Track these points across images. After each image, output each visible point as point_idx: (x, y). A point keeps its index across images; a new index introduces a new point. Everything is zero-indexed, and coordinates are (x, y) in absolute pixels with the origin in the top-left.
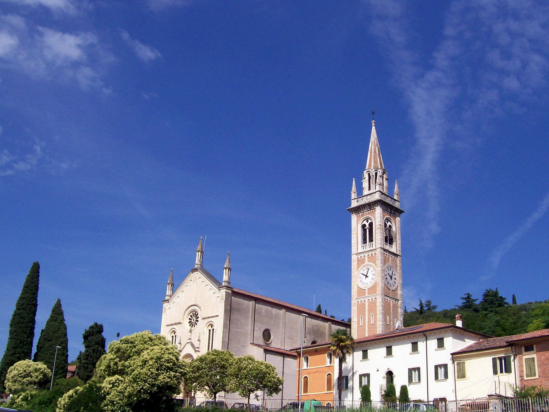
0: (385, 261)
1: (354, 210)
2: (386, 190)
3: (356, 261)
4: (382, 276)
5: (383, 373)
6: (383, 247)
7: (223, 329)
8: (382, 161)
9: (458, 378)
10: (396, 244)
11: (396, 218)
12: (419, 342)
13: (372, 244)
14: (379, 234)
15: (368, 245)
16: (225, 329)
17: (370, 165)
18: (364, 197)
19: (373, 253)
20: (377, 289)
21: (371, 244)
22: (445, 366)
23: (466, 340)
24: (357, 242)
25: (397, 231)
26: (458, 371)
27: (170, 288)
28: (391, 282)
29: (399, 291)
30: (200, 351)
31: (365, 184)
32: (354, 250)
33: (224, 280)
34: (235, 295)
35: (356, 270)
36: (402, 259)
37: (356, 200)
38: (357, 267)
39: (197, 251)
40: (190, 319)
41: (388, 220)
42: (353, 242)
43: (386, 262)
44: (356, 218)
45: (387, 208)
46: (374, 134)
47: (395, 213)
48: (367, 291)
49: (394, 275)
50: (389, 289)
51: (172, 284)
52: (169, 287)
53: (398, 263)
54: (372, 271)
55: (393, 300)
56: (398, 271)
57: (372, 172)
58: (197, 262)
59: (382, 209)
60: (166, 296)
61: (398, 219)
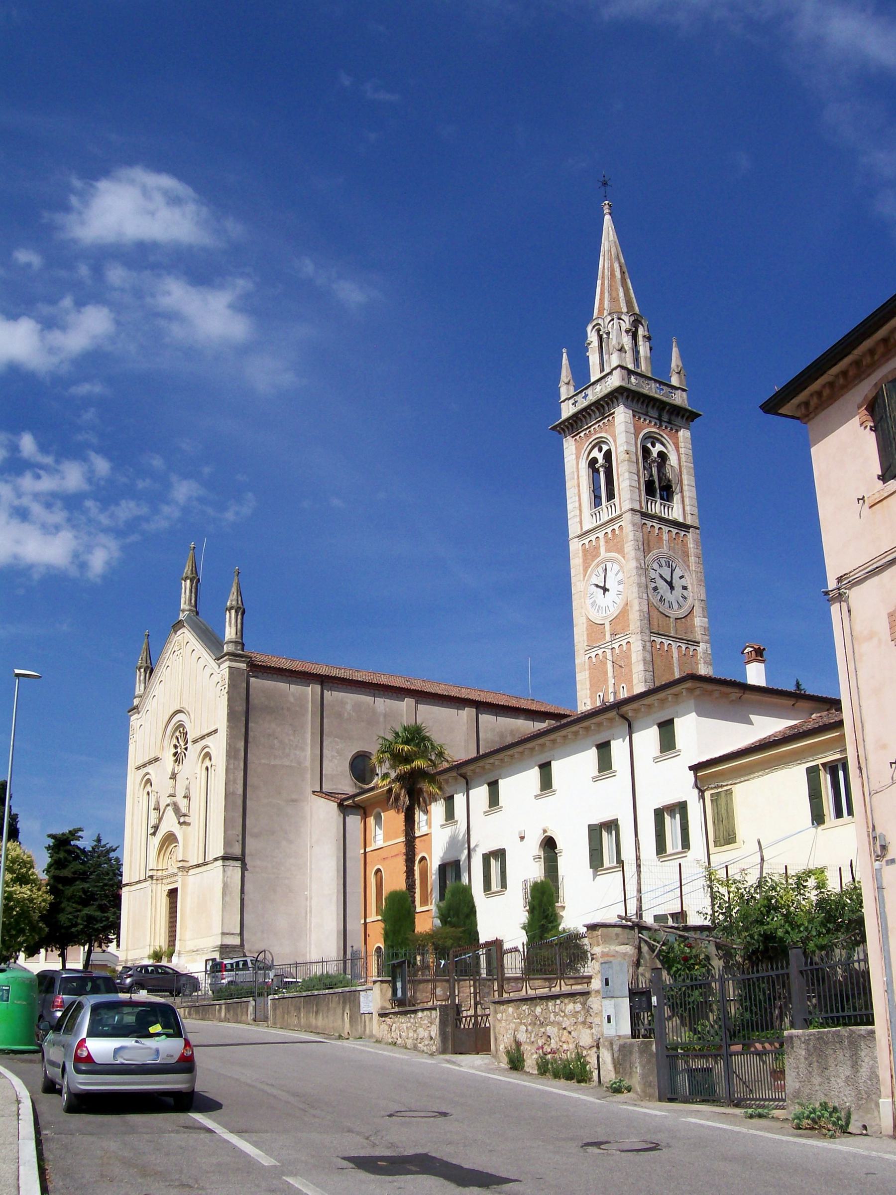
0: (646, 546)
1: (562, 428)
2: (646, 366)
3: (581, 554)
4: (638, 584)
5: (533, 846)
6: (638, 508)
7: (227, 761)
8: (633, 296)
9: (716, 846)
10: (683, 497)
11: (677, 431)
12: (614, 739)
13: (614, 504)
14: (627, 475)
15: (605, 509)
16: (232, 761)
17: (601, 310)
18: (589, 389)
19: (616, 527)
20: (631, 617)
21: (611, 506)
22: (681, 808)
23: (753, 717)
24: (580, 505)
25: (683, 464)
26: (714, 823)
27: (142, 678)
28: (669, 596)
29: (698, 618)
30: (189, 824)
31: (594, 358)
32: (574, 529)
33: (226, 639)
34: (261, 673)
35: (582, 579)
36: (701, 534)
37: (572, 401)
38: (584, 570)
39: (182, 579)
40: (176, 747)
41: (653, 439)
42: (570, 507)
43: (651, 545)
44: (574, 447)
45: (647, 406)
46: (609, 234)
47: (673, 418)
48: (607, 627)
49: (681, 577)
50: (667, 616)
51: (147, 667)
52: (140, 675)
53: (691, 545)
54: (616, 575)
55: (679, 644)
56: (693, 567)
57: (604, 324)
58: (183, 606)
59: (631, 412)
60: (135, 698)
61: (684, 435)
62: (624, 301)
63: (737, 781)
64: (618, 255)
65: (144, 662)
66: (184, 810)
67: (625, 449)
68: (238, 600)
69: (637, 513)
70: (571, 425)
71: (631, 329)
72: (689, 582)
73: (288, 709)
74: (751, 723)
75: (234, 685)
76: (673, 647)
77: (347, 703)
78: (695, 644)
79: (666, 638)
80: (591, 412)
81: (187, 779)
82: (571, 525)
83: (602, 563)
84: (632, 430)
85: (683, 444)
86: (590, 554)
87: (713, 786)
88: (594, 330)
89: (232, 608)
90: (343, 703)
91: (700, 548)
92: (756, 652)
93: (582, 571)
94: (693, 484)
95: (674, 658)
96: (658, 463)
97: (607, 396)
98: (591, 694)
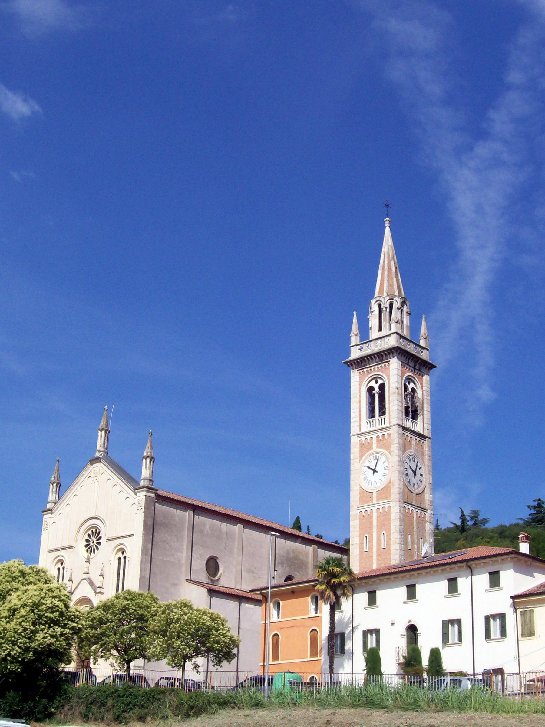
0: (404, 447)
2: (407, 332)
3: (358, 446)
4: (399, 471)
5: (402, 628)
6: (401, 424)
7: (142, 556)
8: (401, 284)
9: (522, 637)
10: (423, 418)
11: (422, 376)
12: (460, 577)
13: (384, 419)
14: (396, 402)
15: (377, 421)
16: (144, 556)
17: (381, 291)
19: (386, 433)
20: (392, 491)
21: (382, 419)
22: (502, 617)
23: (535, 574)
24: (360, 415)
26: (522, 625)
27: (54, 490)
28: (414, 480)
31: (373, 322)
32: (354, 429)
33: (143, 477)
36: (432, 442)
37: (359, 347)
39: (99, 430)
40: (87, 540)
41: (409, 380)
42: (353, 415)
45: (409, 360)
46: (388, 240)
47: (421, 367)
48: (375, 495)
49: (420, 468)
50: (412, 492)
51: (59, 483)
52: (52, 489)
53: (426, 449)
54: (383, 463)
55: (417, 510)
56: (426, 462)
57: (384, 301)
58: (98, 448)
59: (400, 363)
61: (426, 378)
62: (397, 288)
63: (537, 606)
64: (393, 256)
65: (56, 479)
66: (97, 584)
67: (396, 386)
68: (151, 452)
69: (401, 427)
70: (358, 362)
71: (401, 308)
72: (424, 471)
73: (175, 525)
74: (533, 576)
75: (147, 507)
76: (414, 511)
77: (207, 524)
78: (425, 511)
79: (411, 505)
80: (373, 358)
81: (103, 564)
82: (352, 426)
83: (374, 454)
84: (400, 374)
85: (425, 384)
86: (365, 448)
87: (523, 607)
88: (377, 303)
89: (148, 457)
90: (204, 524)
91: (431, 451)
92: (526, 537)
93: (358, 457)
94: (429, 410)
95: (414, 519)
96: (412, 395)
97: (387, 350)
98: (360, 534)
